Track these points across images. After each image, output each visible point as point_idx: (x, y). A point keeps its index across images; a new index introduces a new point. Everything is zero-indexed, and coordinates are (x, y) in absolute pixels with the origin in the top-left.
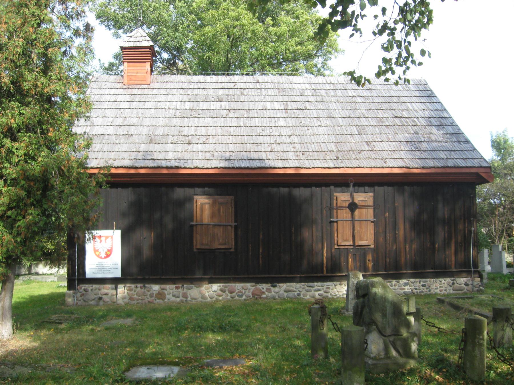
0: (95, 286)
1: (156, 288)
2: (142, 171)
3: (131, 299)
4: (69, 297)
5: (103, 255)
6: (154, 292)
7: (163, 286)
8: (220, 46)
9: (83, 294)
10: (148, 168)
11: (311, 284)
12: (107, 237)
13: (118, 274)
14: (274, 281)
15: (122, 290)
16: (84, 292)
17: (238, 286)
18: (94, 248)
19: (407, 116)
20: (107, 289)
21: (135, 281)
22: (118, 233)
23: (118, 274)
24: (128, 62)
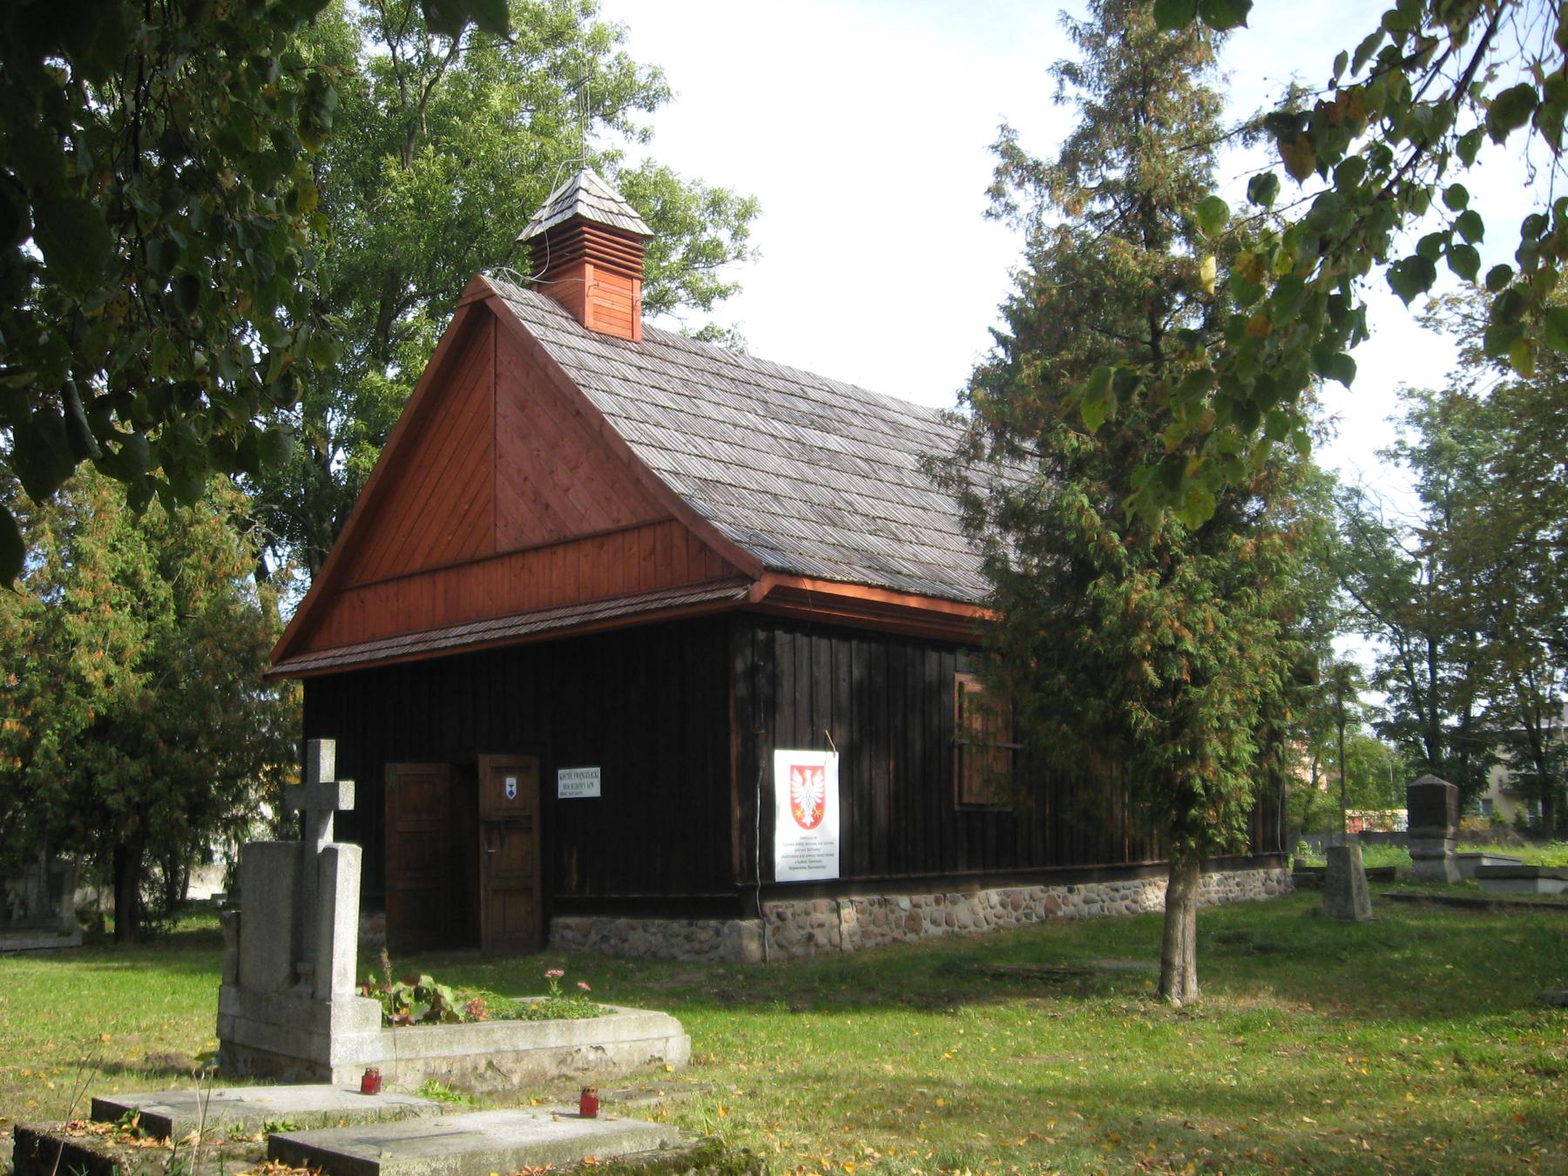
0: (799, 905)
1: (904, 902)
2: (913, 603)
3: (865, 934)
4: (751, 938)
5: (808, 820)
6: (903, 914)
7: (916, 898)
8: (1402, 766)
9: (778, 928)
10: (924, 596)
11: (1119, 884)
12: (814, 769)
13: (831, 871)
14: (1070, 878)
15: (849, 914)
16: (779, 923)
17: (1025, 891)
18: (793, 799)
19: (600, 523)
20: (821, 908)
21: (866, 887)
22: (829, 761)
23: (831, 871)
24: (596, 266)
